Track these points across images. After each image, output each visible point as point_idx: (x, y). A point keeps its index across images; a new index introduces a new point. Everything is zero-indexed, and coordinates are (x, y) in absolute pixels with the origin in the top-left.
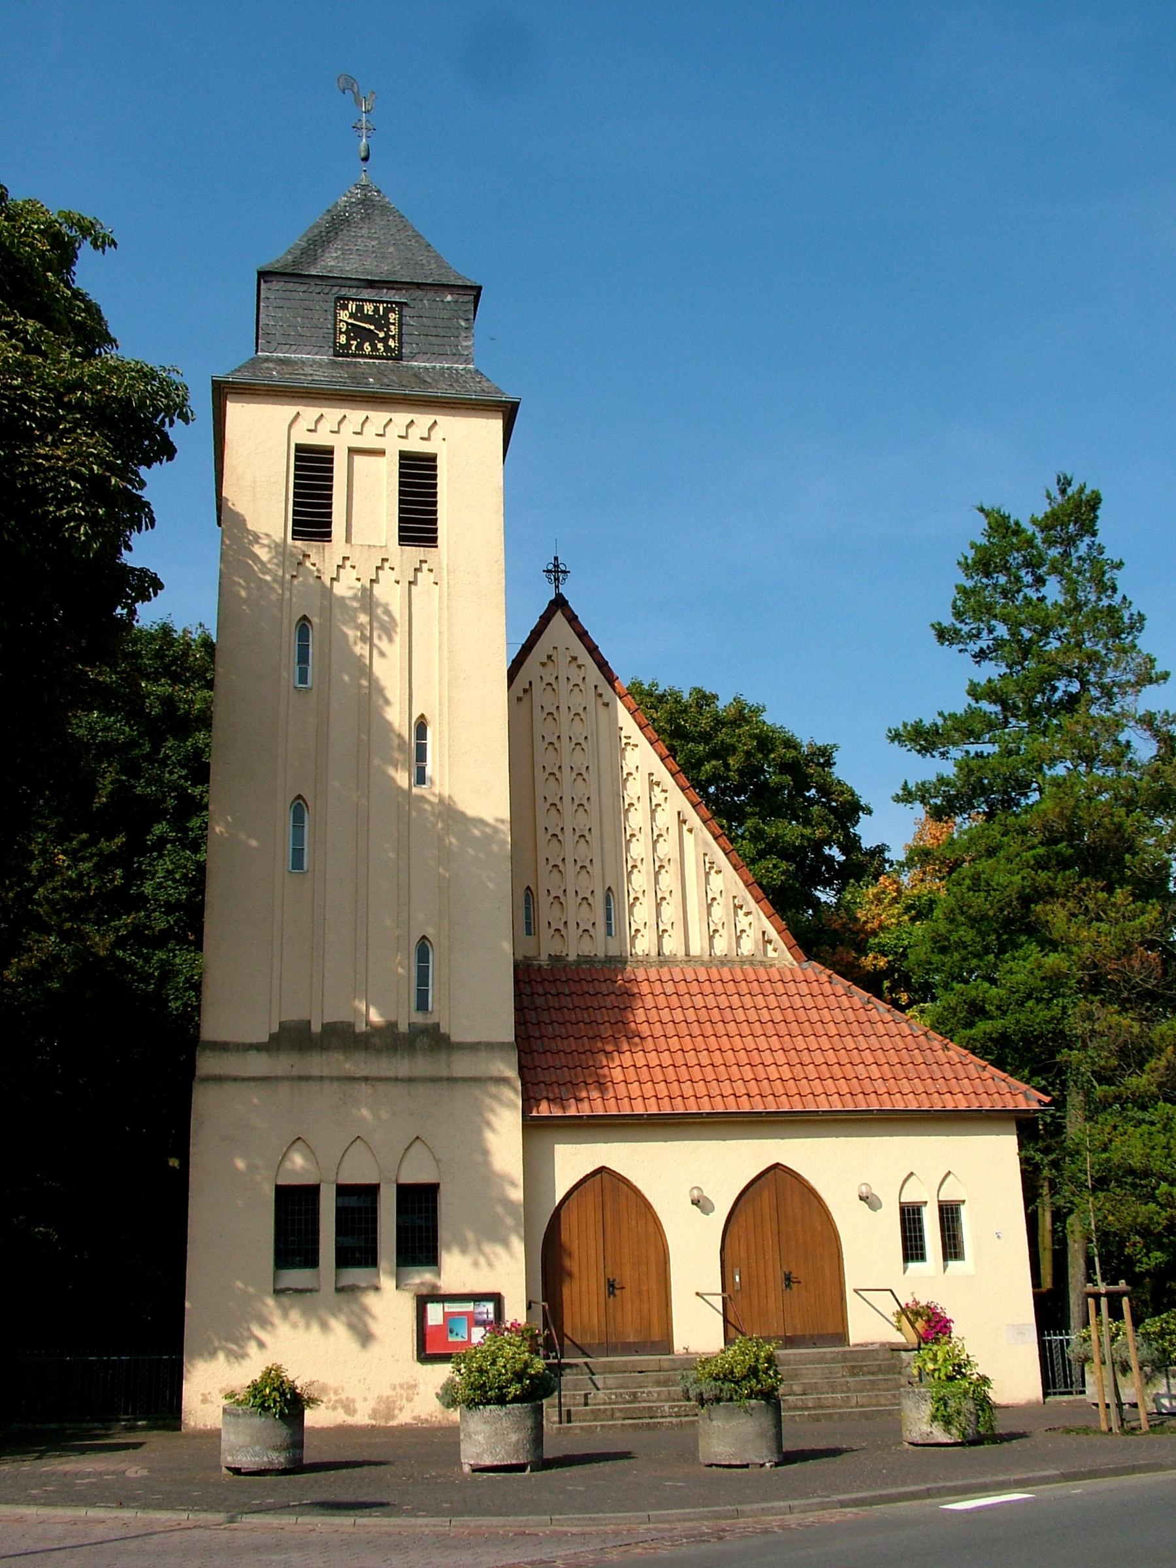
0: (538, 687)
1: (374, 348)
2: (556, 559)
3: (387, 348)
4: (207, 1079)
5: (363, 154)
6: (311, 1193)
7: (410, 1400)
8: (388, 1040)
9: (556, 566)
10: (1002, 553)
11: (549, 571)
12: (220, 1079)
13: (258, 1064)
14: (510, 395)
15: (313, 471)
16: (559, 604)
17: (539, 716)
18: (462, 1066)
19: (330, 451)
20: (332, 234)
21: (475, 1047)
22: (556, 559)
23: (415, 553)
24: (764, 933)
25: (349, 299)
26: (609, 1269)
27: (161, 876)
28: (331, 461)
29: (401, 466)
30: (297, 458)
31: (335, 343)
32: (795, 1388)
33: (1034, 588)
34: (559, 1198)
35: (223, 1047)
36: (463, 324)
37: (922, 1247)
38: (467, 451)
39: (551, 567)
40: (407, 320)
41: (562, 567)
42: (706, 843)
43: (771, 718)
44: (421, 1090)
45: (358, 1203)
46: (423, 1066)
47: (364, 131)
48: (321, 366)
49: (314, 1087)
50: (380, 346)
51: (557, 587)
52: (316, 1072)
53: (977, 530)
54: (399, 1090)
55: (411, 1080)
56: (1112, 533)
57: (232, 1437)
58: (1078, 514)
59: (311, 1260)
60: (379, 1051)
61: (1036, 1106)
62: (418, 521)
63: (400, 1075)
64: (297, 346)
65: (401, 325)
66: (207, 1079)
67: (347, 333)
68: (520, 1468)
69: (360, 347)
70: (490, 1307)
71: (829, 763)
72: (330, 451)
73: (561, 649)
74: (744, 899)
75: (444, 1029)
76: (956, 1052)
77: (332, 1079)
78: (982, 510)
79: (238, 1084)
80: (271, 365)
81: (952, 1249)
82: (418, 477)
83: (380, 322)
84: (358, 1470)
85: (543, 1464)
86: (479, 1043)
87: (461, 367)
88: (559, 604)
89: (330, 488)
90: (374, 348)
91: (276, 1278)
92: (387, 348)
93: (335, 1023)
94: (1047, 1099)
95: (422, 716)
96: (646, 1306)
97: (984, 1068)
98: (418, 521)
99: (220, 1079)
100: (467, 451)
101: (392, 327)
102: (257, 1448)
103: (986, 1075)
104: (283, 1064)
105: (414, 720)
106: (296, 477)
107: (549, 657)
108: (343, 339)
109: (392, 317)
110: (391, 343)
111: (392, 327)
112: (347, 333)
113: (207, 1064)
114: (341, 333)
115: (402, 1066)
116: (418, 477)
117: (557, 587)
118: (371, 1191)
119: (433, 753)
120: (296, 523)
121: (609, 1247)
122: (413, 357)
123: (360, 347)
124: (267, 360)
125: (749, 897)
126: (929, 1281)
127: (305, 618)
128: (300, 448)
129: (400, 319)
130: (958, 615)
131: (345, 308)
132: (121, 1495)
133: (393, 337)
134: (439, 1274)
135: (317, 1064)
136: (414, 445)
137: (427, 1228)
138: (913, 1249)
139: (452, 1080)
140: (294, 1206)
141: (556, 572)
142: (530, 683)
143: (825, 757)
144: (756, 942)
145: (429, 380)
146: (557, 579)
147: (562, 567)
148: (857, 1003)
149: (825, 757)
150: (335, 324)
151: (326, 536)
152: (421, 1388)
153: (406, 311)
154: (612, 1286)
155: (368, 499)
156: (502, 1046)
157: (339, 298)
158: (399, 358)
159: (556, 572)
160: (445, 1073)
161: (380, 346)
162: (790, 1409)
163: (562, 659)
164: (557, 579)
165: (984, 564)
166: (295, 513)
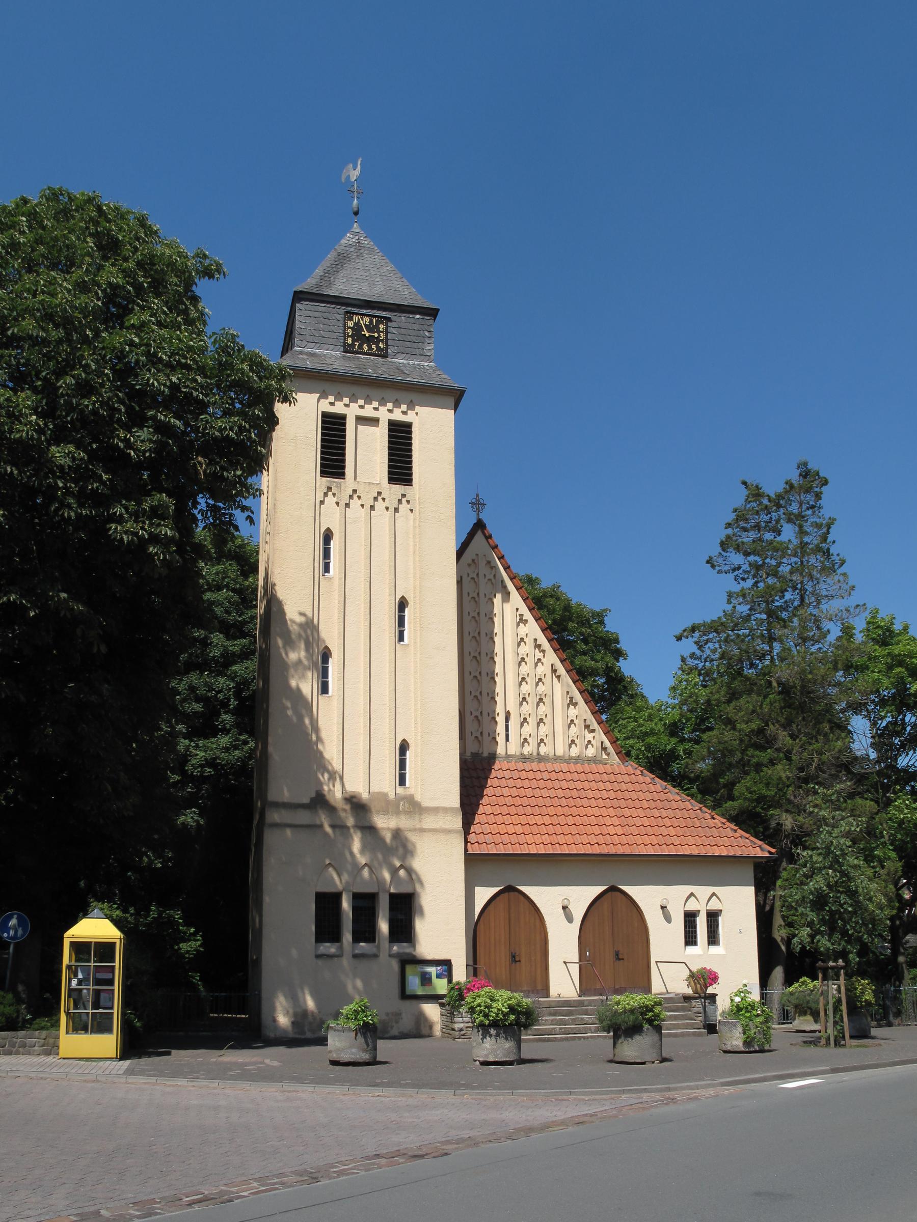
1: (370, 348)
2: (477, 495)
3: (378, 348)
5: (356, 209)
7: (397, 1022)
15: (333, 431)
16: (479, 526)
18: (429, 822)
19: (343, 417)
21: (436, 810)
22: (477, 495)
23: (398, 489)
24: (602, 743)
28: (344, 424)
29: (390, 430)
30: (323, 422)
31: (344, 343)
33: (777, 536)
35: (277, 805)
36: (427, 334)
37: (696, 937)
38: (433, 428)
39: (474, 501)
42: (568, 686)
45: (365, 904)
48: (336, 358)
50: (374, 346)
51: (478, 514)
53: (739, 497)
56: (832, 503)
57: (337, 1043)
58: (810, 481)
59: (336, 937)
61: (767, 855)
62: (400, 468)
64: (321, 344)
65: (387, 333)
68: (511, 1063)
69: (361, 347)
71: (602, 623)
72: (343, 417)
74: (591, 721)
75: (418, 798)
76: (719, 820)
78: (744, 483)
80: (305, 357)
81: (713, 939)
82: (400, 439)
85: (522, 1061)
86: (437, 808)
87: (426, 364)
88: (479, 526)
89: (344, 443)
90: (370, 348)
91: (316, 948)
92: (378, 348)
94: (773, 850)
95: (403, 597)
97: (736, 831)
98: (400, 468)
100: (433, 428)
102: (354, 1050)
103: (737, 835)
105: (397, 600)
106: (323, 434)
107: (473, 561)
108: (350, 341)
109: (381, 326)
110: (381, 345)
113: (274, 816)
114: (349, 336)
116: (400, 439)
117: (478, 514)
119: (410, 623)
120: (322, 465)
123: (361, 347)
124: (301, 353)
125: (594, 720)
126: (701, 955)
127: (328, 529)
128: (325, 415)
129: (387, 328)
131: (351, 319)
132: (246, 1075)
134: (414, 946)
136: (397, 416)
138: (690, 939)
143: (600, 617)
144: (597, 749)
148: (659, 788)
149: (600, 617)
150: (345, 330)
151: (341, 475)
152: (404, 1015)
153: (390, 324)
155: (368, 450)
156: (452, 810)
157: (347, 312)
158: (385, 356)
159: (478, 504)
160: (418, 826)
161: (374, 346)
164: (478, 509)
166: (322, 459)
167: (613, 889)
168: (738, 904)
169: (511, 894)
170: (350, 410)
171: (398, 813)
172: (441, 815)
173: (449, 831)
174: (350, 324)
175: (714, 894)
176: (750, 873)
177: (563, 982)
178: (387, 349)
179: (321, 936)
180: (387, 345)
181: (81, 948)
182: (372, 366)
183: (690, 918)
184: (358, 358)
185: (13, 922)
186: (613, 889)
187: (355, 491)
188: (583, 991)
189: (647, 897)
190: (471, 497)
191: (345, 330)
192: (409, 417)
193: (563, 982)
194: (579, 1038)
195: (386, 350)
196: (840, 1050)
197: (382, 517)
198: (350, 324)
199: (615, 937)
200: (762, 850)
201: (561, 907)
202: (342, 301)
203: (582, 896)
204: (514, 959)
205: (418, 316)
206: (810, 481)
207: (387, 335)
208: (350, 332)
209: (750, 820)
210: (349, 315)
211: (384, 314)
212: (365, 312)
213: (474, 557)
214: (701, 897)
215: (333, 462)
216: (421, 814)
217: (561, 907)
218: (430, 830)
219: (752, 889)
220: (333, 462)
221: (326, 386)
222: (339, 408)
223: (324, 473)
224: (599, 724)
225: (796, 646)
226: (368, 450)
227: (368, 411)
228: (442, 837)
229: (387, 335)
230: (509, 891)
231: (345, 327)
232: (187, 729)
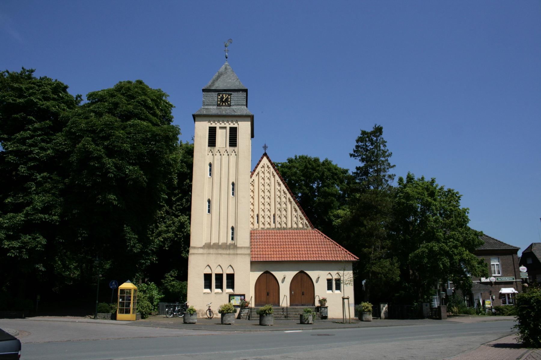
0: (260, 173)
4: (191, 254)
6: (210, 275)
8: (225, 247)
10: (364, 137)
12: (194, 254)
13: (201, 251)
14: (251, 114)
15: (212, 132)
17: (260, 178)
18: (239, 251)
21: (241, 248)
23: (232, 148)
27: (163, 231)
34: (272, 272)
35: (194, 248)
43: (334, 163)
44: (231, 256)
45: (219, 277)
46: (231, 251)
49: (211, 255)
52: (211, 252)
54: (227, 256)
55: (229, 254)
56: (385, 136)
58: (378, 130)
60: (223, 249)
66: (191, 254)
72: (215, 128)
82: (233, 132)
83: (223, 101)
88: (265, 154)
99: (194, 254)
104: (205, 251)
108: (219, 103)
115: (228, 252)
122: (233, 106)
128: (210, 127)
130: (354, 151)
139: (237, 254)
140: (208, 277)
141: (265, 147)
154: (268, 295)
155: (222, 137)
159: (265, 147)
163: (266, 166)
165: (360, 140)
167: (302, 272)
168: (348, 275)
170: (218, 125)
171: (230, 249)
173: (246, 254)
174: (219, 97)
175: (330, 273)
176: (351, 267)
177: (285, 301)
179: (206, 287)
181: (123, 291)
182: (225, 110)
183: (329, 281)
185: (114, 283)
186: (302, 272)
189: (313, 274)
192: (236, 125)
193: (285, 301)
196: (261, 332)
197: (225, 158)
199: (303, 287)
201: (285, 278)
203: (290, 275)
206: (378, 130)
209: (350, 248)
210: (219, 95)
214: (334, 275)
215: (212, 142)
217: (285, 278)
218: (240, 254)
219: (351, 272)
220: (212, 142)
221: (210, 119)
222: (213, 125)
223: (209, 146)
225: (182, 162)
226: (222, 137)
227: (223, 125)
228: (243, 256)
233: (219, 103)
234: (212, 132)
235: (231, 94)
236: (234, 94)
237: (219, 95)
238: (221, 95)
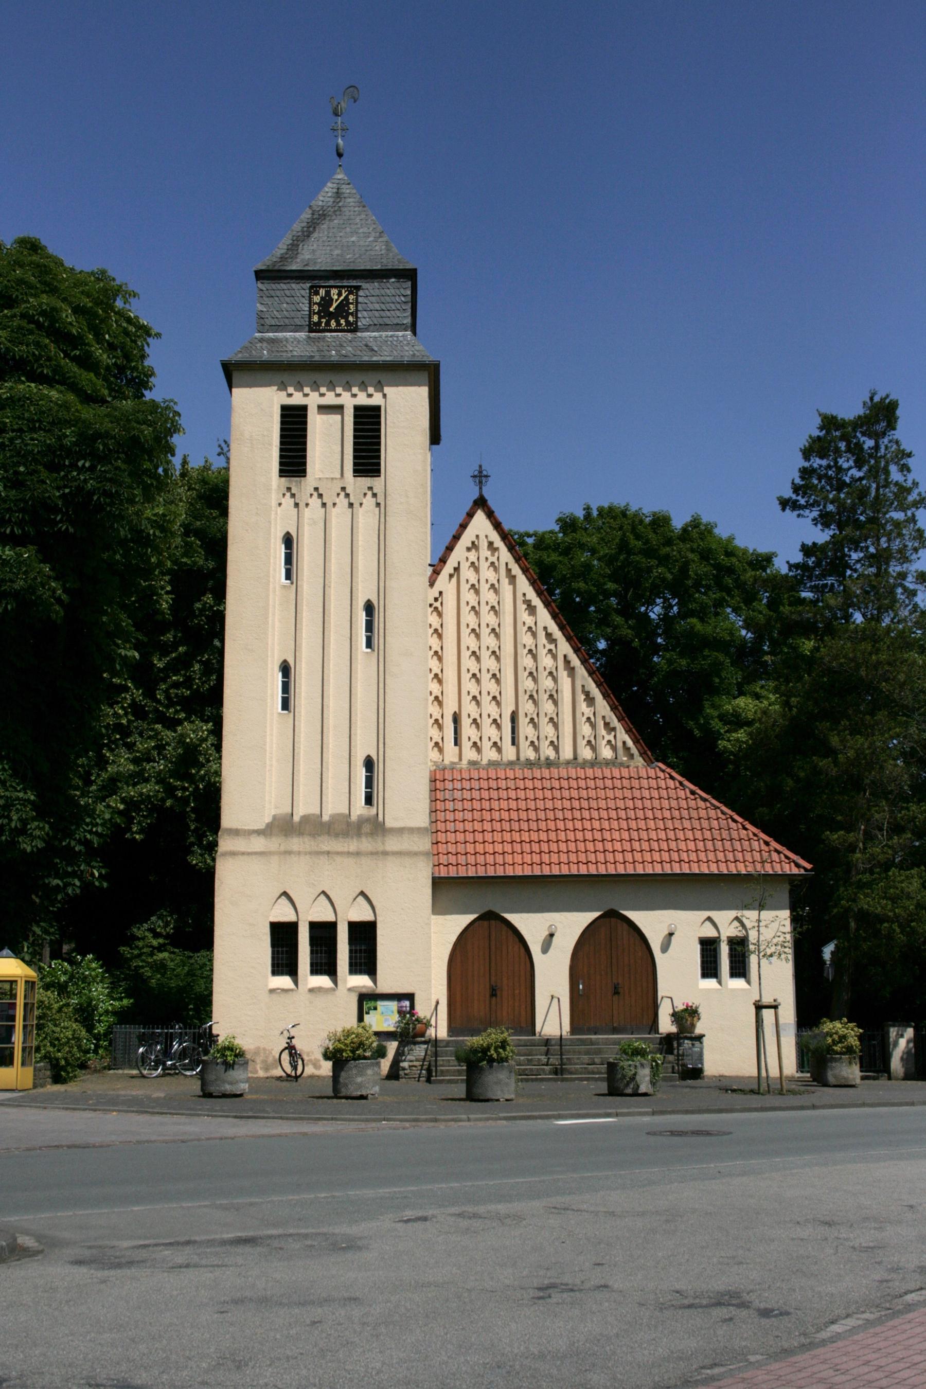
0: (465, 566)
1: (338, 324)
2: (480, 466)
3: (348, 322)
4: (225, 854)
9: (480, 472)
10: (832, 436)
11: (474, 476)
12: (233, 854)
13: (258, 844)
15: (294, 423)
17: (465, 587)
18: (392, 844)
19: (304, 408)
20: (311, 229)
21: (401, 831)
22: (480, 466)
23: (365, 482)
25: (320, 287)
26: (493, 979)
27: (122, 780)
31: (310, 321)
32: (596, 1060)
34: (508, 916)
35: (236, 832)
39: (476, 473)
40: (360, 299)
41: (485, 473)
43: (722, 532)
45: (323, 934)
46: (366, 844)
47: (340, 132)
49: (294, 858)
50: (343, 321)
51: (481, 488)
52: (295, 848)
54: (350, 861)
55: (358, 854)
58: (883, 413)
60: (337, 835)
61: (802, 872)
62: (367, 457)
63: (351, 850)
66: (225, 854)
67: (318, 313)
70: (407, 1003)
72: (304, 408)
73: (482, 537)
74: (610, 718)
77: (306, 853)
79: (245, 857)
82: (368, 423)
84: (568, 1083)
88: (481, 503)
90: (338, 324)
93: (309, 815)
96: (517, 1004)
98: (367, 457)
99: (233, 854)
100: (404, 409)
101: (351, 306)
107: (473, 543)
108: (315, 318)
110: (351, 319)
111: (351, 306)
112: (318, 313)
114: (315, 313)
115: (353, 845)
117: (481, 488)
118: (331, 927)
121: (493, 964)
122: (366, 329)
128: (284, 408)
129: (357, 299)
131: (317, 293)
133: (352, 314)
135: (295, 843)
136: (362, 399)
137: (356, 952)
139: (385, 853)
140: (283, 935)
141: (480, 477)
142: (459, 563)
145: (376, 349)
146: (481, 482)
147: (485, 473)
155: (328, 442)
156: (419, 830)
158: (355, 330)
159: (480, 477)
160: (381, 849)
162: (456, 1082)
163: (484, 545)
164: (481, 482)
168: (773, 926)
169: (493, 922)
170: (312, 399)
171: (359, 834)
172: (406, 836)
174: (317, 299)
175: (709, 919)
176: (784, 896)
177: (553, 1016)
178: (357, 322)
180: (357, 317)
182: (336, 345)
183: (709, 947)
184: (324, 338)
187: (316, 489)
188: (574, 1029)
189: (651, 922)
190: (474, 470)
191: (310, 307)
192: (376, 400)
193: (553, 1016)
194: (532, 1080)
195: (356, 324)
197: (339, 515)
198: (317, 299)
199: (615, 967)
200: (798, 865)
201: (553, 937)
202: (306, 274)
203: (571, 924)
204: (493, 993)
205: (393, 280)
206: (883, 413)
207: (357, 306)
208: (316, 308)
210: (314, 290)
211: (354, 283)
212: (332, 283)
213: (474, 539)
214: (726, 923)
215: (293, 461)
216: (384, 836)
217: (553, 937)
219: (785, 914)
220: (293, 461)
222: (297, 399)
224: (619, 721)
226: (328, 442)
227: (330, 399)
228: (407, 861)
229: (357, 306)
230: (489, 919)
231: (310, 304)
232: (618, 604)
233: (315, 318)
234: (294, 423)
235: (358, 288)
236: (369, 288)
237: (314, 290)
238: (322, 292)
